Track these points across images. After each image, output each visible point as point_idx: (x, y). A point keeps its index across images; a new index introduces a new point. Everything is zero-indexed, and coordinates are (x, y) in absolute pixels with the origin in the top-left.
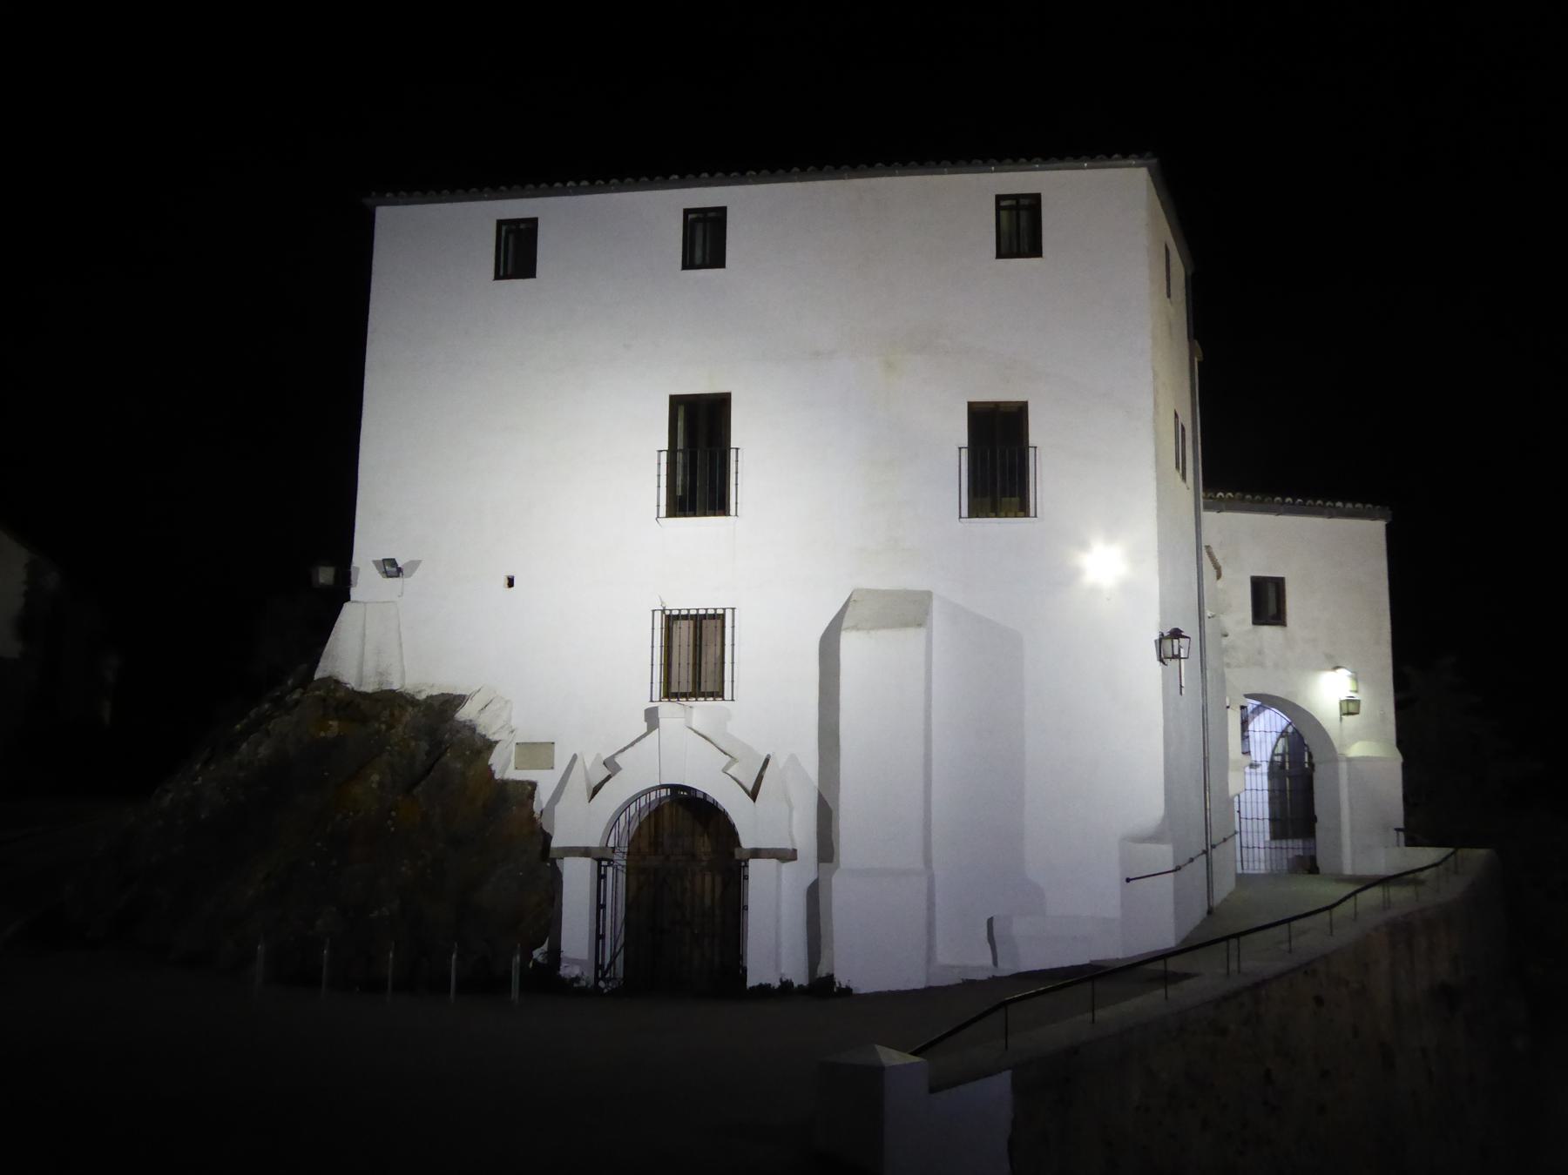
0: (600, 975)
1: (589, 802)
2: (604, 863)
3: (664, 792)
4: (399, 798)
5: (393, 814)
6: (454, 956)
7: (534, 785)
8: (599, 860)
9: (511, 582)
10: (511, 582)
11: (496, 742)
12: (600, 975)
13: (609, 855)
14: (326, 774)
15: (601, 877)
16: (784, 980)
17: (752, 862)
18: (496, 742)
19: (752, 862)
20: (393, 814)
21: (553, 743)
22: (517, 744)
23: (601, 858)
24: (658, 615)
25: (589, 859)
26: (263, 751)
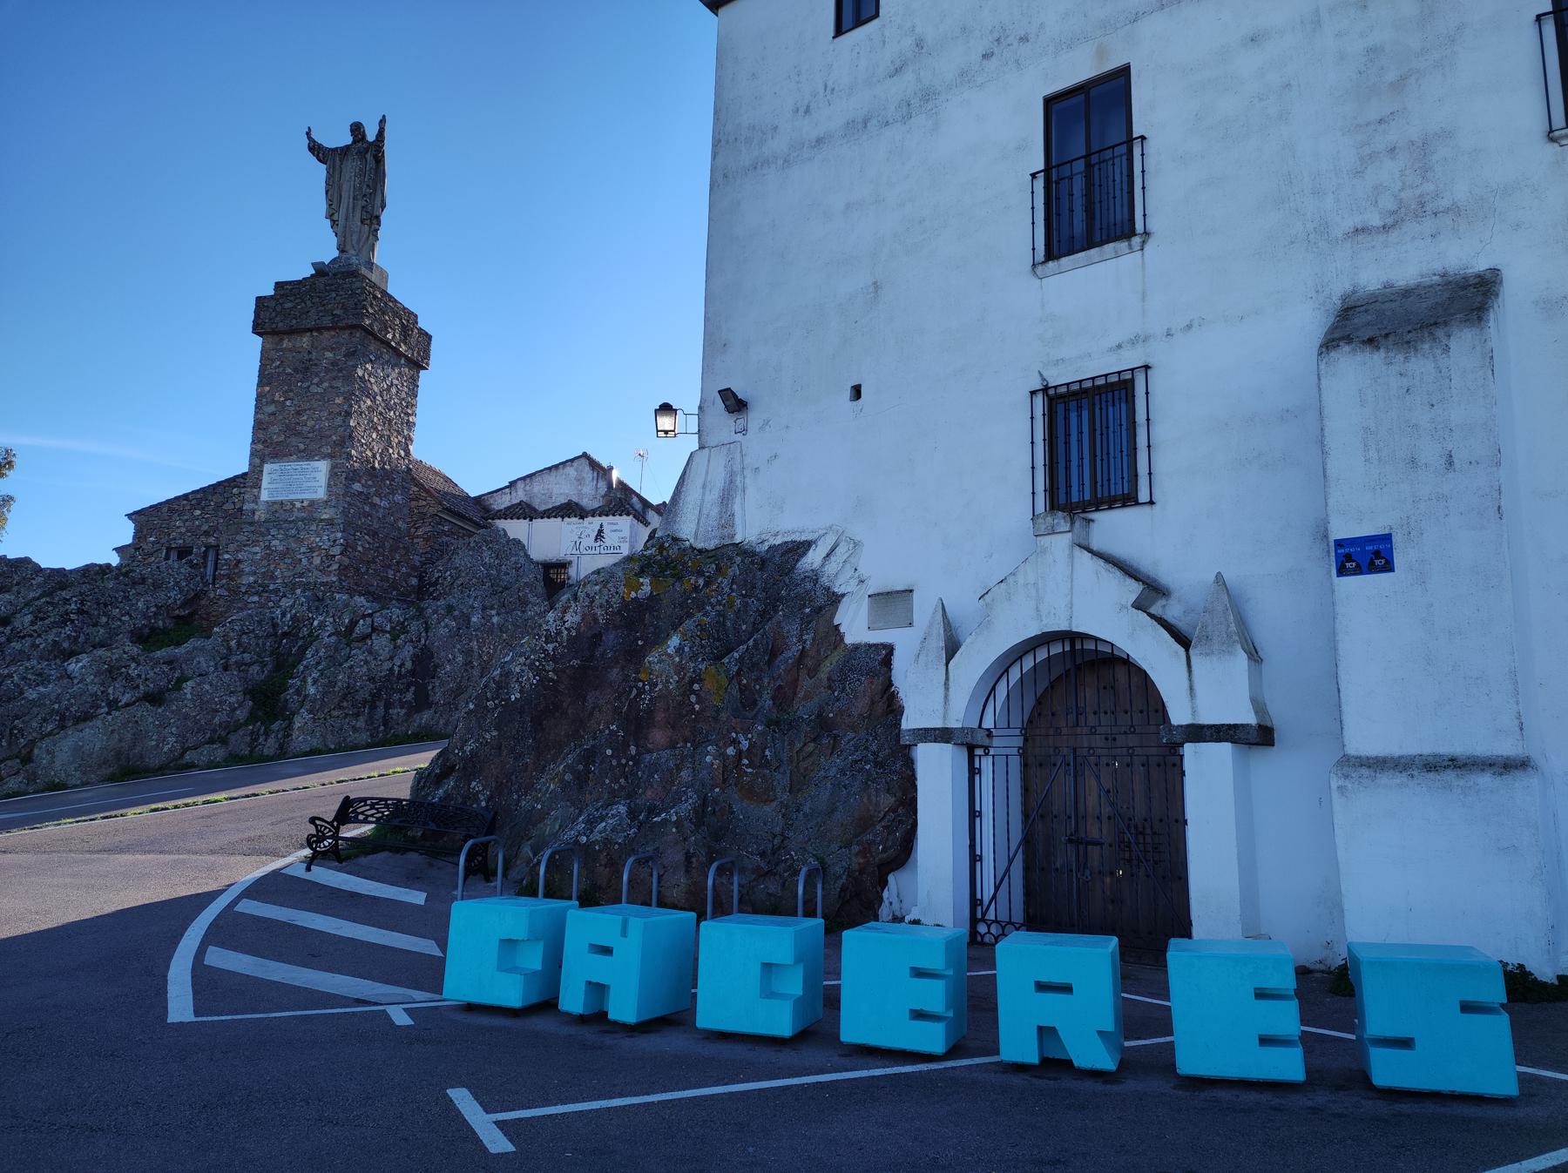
0: (979, 916)
1: (384, 116)
2: (979, 752)
3: (1056, 649)
4: (702, 667)
5: (696, 687)
6: (576, 866)
7: (889, 649)
8: (971, 748)
9: (857, 392)
10: (857, 392)
11: (843, 595)
12: (979, 916)
13: (980, 738)
14: (640, 643)
15: (973, 772)
16: (1045, 1056)
17: (1189, 749)
18: (843, 595)
19: (1189, 749)
20: (696, 687)
21: (911, 591)
22: (869, 596)
23: (972, 744)
24: (1039, 400)
25: (950, 746)
26: (572, 618)
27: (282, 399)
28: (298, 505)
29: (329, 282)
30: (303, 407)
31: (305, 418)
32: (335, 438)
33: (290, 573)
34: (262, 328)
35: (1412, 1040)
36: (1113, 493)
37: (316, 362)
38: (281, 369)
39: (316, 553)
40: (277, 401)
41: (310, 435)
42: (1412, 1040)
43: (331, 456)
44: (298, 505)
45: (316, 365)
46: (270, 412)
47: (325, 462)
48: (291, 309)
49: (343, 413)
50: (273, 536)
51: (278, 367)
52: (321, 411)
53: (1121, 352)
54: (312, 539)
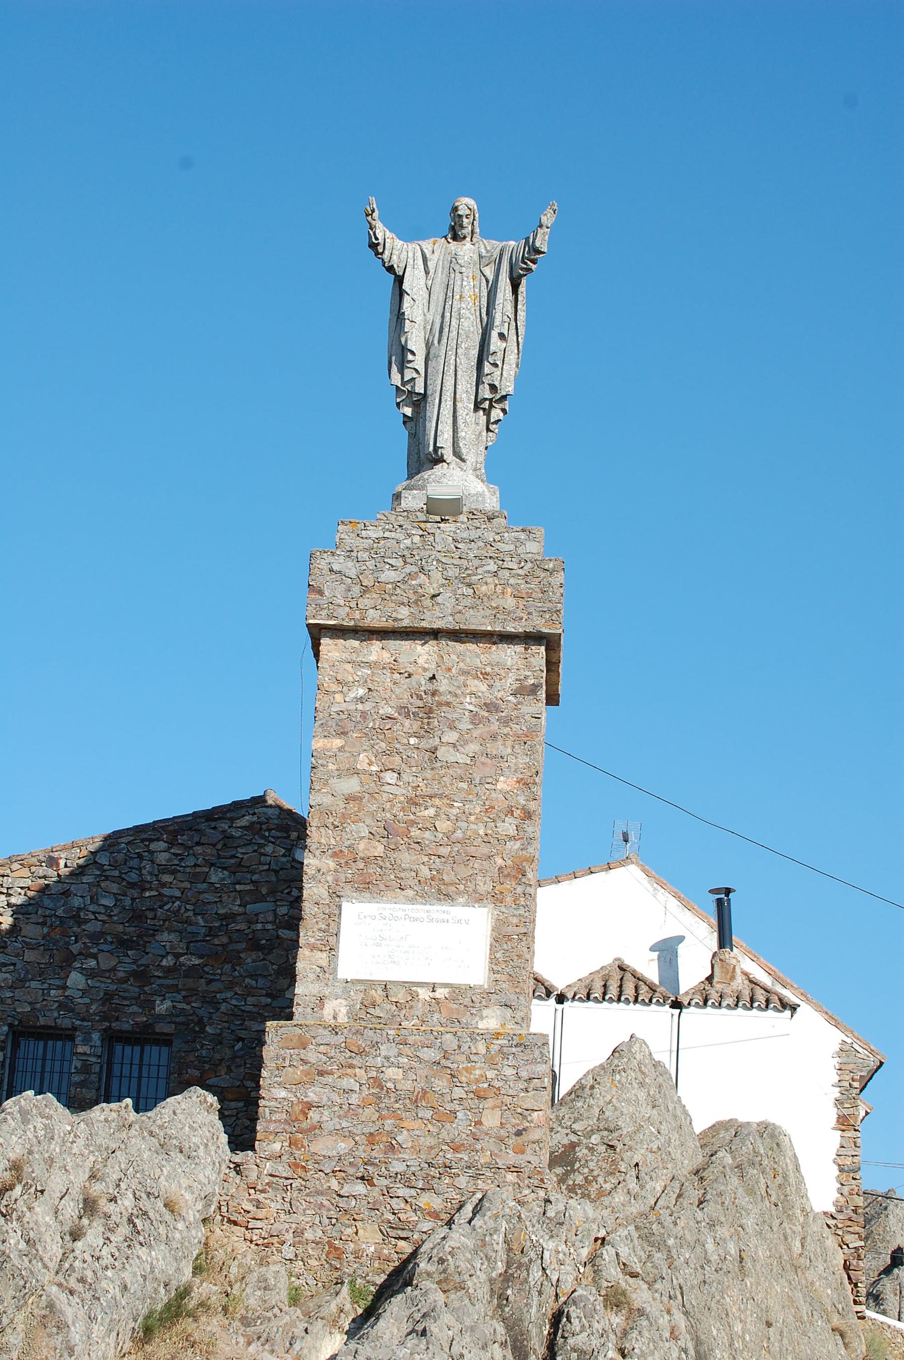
27: (374, 768)
28: (424, 994)
29: (465, 535)
30: (425, 790)
31: (431, 812)
32: (500, 862)
33: (430, 1141)
34: (330, 617)
35: (557, 704)
36: (41, 1043)
37: (449, 698)
38: (368, 706)
39: (490, 1103)
40: (365, 772)
41: (444, 851)
42: (557, 704)
43: (496, 898)
44: (424, 994)
45: (448, 704)
46: (346, 792)
47: (486, 910)
48: (396, 585)
49: (517, 813)
50: (387, 1058)
51: (361, 700)
52: (464, 801)
53: (733, 1142)
54: (478, 1072)
